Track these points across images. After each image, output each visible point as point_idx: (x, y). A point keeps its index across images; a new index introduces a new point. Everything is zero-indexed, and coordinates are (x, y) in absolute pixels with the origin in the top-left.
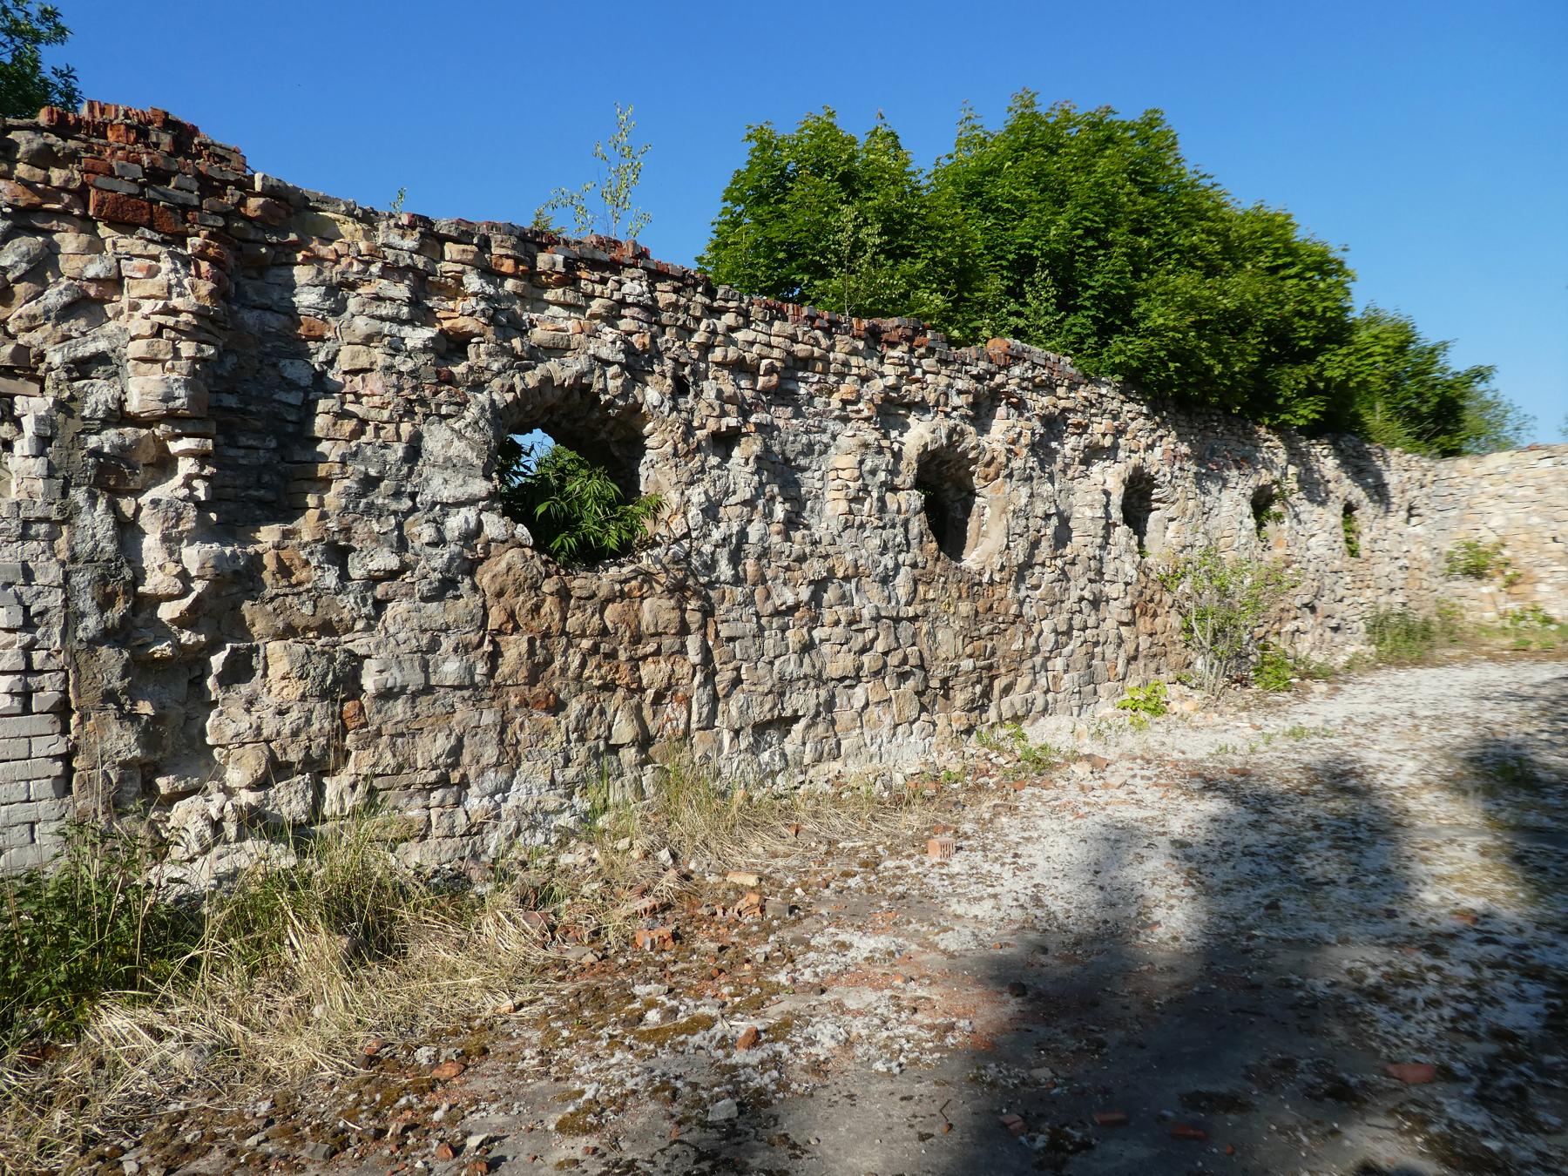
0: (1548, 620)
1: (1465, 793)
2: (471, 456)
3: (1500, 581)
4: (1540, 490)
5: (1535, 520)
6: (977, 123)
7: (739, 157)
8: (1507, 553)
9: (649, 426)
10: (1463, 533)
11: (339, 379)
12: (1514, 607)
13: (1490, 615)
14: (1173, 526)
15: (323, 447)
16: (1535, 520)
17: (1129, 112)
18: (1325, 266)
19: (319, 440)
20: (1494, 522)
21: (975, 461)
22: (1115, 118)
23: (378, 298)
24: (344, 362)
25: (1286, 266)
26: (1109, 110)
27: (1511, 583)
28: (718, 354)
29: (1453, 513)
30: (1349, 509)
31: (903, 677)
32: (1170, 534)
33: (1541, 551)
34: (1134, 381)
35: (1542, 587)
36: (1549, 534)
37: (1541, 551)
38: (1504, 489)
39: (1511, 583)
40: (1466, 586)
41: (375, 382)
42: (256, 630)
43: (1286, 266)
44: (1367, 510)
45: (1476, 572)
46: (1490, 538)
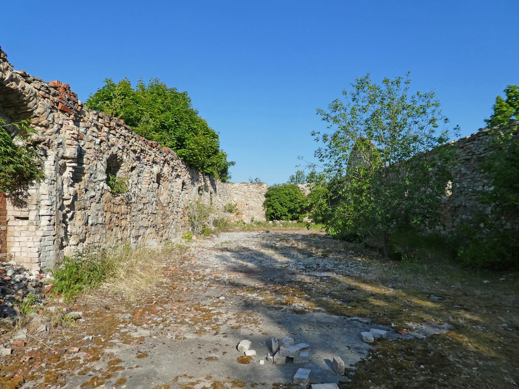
0: (244, 223)
1: (397, 257)
2: (104, 169)
3: (235, 213)
4: (245, 193)
5: (243, 200)
6: (142, 82)
7: (102, 85)
8: (237, 207)
9: (123, 164)
10: (228, 201)
11: (85, 149)
12: (238, 220)
13: (233, 221)
14: (187, 195)
15: (84, 166)
16: (243, 200)
17: (180, 91)
18: (215, 136)
19: (83, 164)
20: (235, 199)
21: (162, 177)
22: (177, 91)
23: (94, 132)
24: (86, 146)
25: (207, 134)
26: (175, 89)
27: (237, 214)
28: (132, 148)
29: (226, 196)
30: (211, 193)
31: (154, 227)
32: (186, 197)
33: (244, 207)
34: (185, 160)
35: (243, 216)
36: (246, 203)
37: (244, 207)
38: (237, 192)
39: (237, 214)
40: (228, 214)
41: (92, 151)
42: (76, 208)
43: (207, 134)
44: (214, 194)
45: (231, 211)
46: (234, 203)
